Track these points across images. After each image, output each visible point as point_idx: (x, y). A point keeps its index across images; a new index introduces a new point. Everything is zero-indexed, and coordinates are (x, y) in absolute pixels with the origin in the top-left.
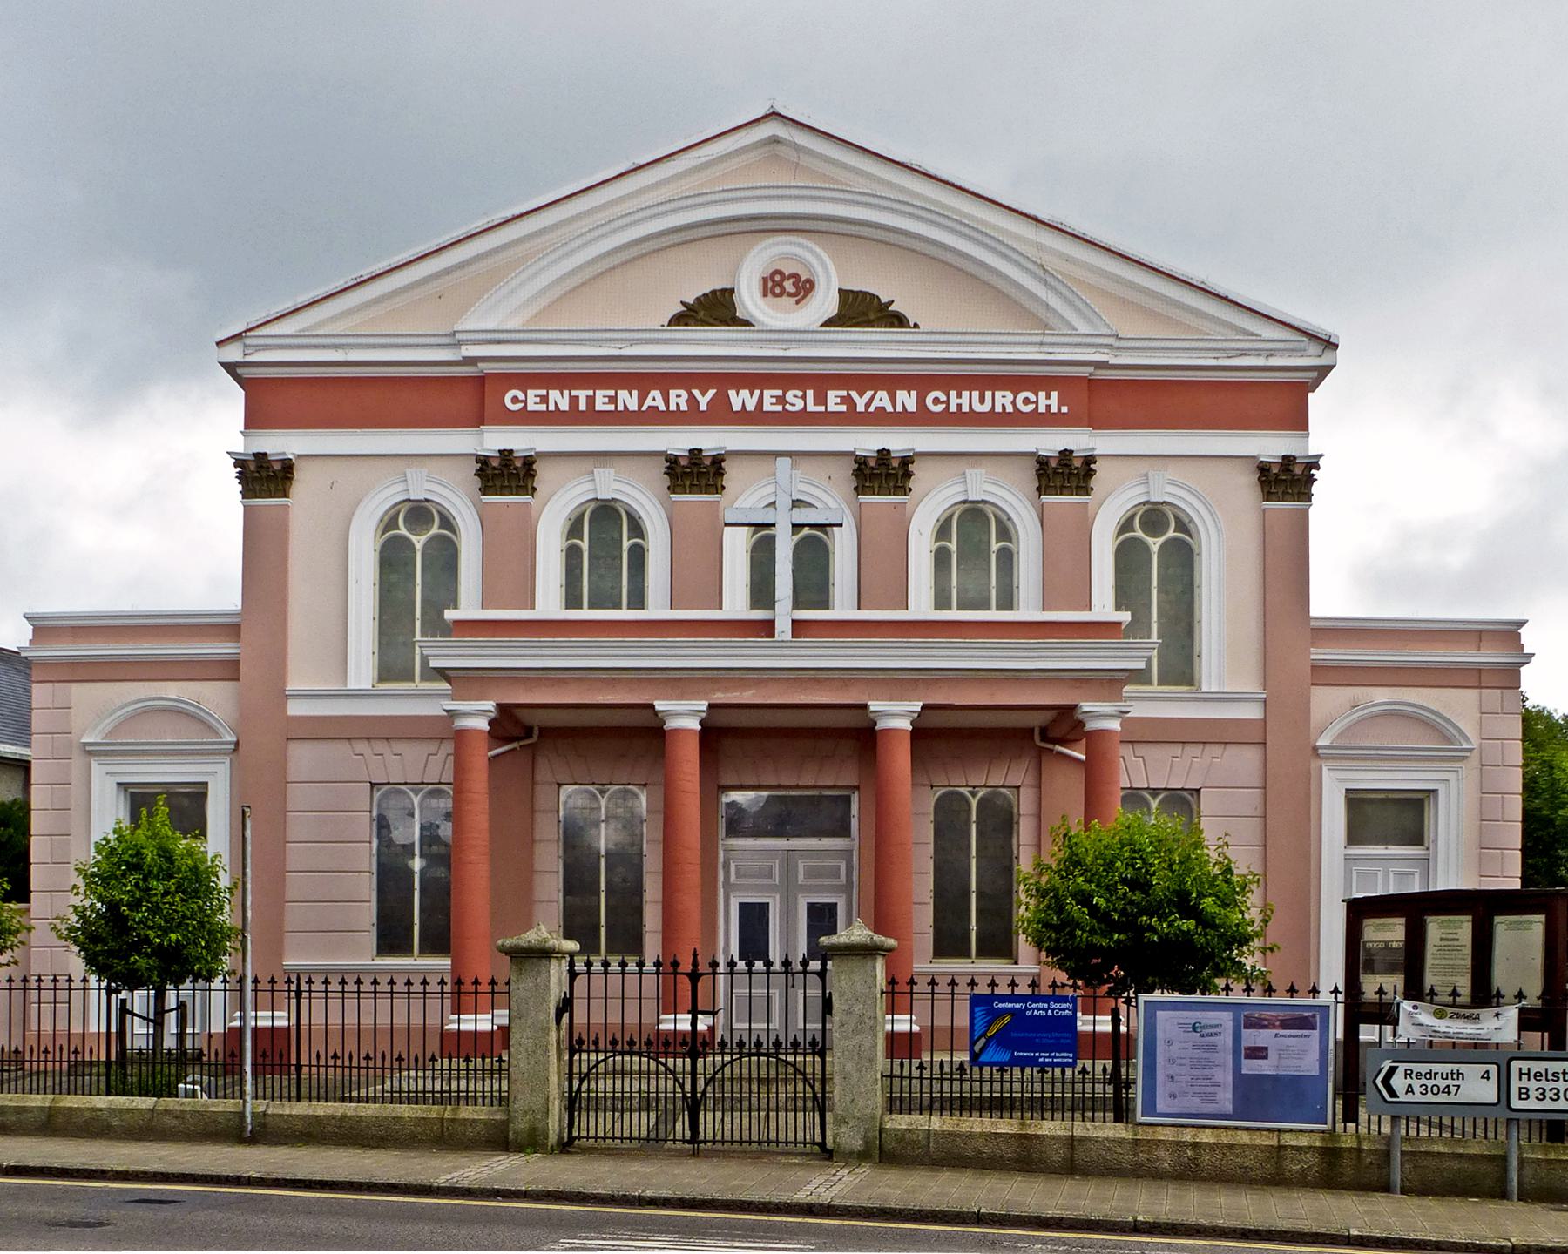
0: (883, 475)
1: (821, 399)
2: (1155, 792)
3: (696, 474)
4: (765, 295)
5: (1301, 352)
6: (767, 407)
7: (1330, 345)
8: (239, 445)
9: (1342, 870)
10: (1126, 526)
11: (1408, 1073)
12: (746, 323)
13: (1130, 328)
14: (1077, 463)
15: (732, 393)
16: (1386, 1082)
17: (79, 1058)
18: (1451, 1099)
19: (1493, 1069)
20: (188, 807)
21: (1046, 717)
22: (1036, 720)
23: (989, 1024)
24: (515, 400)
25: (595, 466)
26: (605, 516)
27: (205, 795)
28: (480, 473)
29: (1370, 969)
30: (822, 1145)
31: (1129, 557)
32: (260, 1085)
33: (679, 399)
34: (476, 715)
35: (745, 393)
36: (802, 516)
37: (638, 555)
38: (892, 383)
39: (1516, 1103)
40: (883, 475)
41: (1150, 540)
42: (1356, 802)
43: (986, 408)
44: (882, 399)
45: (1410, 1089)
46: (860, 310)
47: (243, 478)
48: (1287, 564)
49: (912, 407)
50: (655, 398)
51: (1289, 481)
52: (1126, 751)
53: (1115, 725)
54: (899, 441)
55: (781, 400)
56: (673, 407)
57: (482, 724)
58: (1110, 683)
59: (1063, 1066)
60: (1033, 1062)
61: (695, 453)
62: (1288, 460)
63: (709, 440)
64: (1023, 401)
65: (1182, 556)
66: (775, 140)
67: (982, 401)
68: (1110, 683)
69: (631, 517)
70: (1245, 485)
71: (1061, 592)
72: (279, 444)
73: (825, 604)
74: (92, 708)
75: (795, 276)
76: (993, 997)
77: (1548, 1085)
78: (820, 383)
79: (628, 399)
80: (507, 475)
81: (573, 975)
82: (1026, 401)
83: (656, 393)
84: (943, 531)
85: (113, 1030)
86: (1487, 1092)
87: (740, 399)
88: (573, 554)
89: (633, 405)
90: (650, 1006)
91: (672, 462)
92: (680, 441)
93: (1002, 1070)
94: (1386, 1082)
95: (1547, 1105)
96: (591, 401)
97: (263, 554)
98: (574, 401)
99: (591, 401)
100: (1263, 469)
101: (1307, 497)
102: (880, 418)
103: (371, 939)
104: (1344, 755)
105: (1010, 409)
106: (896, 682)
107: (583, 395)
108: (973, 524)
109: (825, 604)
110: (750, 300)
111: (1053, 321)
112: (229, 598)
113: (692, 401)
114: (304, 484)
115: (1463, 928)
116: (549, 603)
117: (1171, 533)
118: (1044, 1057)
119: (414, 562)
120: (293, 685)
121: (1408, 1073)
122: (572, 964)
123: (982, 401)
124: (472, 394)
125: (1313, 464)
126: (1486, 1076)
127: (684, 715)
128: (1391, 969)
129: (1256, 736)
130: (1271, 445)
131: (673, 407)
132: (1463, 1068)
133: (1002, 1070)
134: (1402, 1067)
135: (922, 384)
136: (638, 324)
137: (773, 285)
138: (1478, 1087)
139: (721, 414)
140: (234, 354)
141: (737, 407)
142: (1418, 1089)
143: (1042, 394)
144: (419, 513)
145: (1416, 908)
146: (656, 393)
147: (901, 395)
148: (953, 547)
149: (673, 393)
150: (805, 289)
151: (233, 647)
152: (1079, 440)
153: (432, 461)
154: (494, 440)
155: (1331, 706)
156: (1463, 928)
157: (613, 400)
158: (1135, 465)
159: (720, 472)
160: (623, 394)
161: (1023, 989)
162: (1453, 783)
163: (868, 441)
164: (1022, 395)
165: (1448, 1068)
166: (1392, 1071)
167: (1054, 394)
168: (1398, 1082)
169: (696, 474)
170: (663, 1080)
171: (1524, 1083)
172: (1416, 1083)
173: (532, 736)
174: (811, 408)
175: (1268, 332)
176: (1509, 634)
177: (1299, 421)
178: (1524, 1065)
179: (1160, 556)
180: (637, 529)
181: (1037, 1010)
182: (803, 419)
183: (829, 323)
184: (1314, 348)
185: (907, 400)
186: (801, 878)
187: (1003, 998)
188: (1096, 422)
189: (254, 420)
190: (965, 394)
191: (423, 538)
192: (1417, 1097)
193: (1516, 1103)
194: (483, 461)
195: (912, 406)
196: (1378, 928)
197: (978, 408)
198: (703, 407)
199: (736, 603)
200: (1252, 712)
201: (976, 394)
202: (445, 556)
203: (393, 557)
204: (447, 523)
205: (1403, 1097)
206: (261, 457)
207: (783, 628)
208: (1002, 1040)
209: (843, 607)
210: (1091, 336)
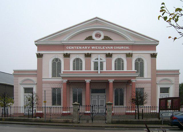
0: (109, 56)
1: (102, 48)
2: (57, 88)
3: (88, 56)
4: (96, 36)
5: (156, 42)
8: (37, 52)
9: (159, 95)
10: (136, 60)
13: (137, 40)
14: (131, 54)
20: (59, 89)
21: (127, 81)
22: (126, 81)
28: (64, 55)
31: (136, 64)
33: (86, 47)
36: (101, 61)
40: (109, 56)
41: (139, 62)
42: (161, 89)
44: (109, 47)
46: (106, 38)
47: (37, 56)
51: (154, 56)
52: (136, 84)
54: (111, 52)
55: (98, 48)
56: (85, 48)
58: (135, 77)
61: (88, 53)
63: (90, 52)
64: (125, 48)
65: (142, 64)
66: (97, 20)
68: (135, 77)
69: (80, 60)
70: (149, 56)
71: (128, 69)
72: (41, 52)
74: (21, 79)
79: (80, 48)
80: (67, 56)
82: (125, 48)
84: (116, 61)
89: (81, 48)
90: (61, 111)
91: (106, 54)
92: (86, 52)
96: (76, 48)
98: (74, 48)
99: (76, 48)
101: (156, 57)
102: (108, 49)
103: (51, 104)
104: (160, 84)
107: (75, 47)
108: (119, 61)
110: (94, 37)
112: (35, 68)
113: (88, 48)
114: (44, 56)
116: (71, 70)
120: (43, 78)
124: (63, 46)
125: (156, 54)
130: (152, 52)
131: (85, 48)
136: (81, 40)
139: (91, 49)
140: (36, 43)
144: (57, 60)
145: (167, 99)
146: (109, 47)
147: (111, 47)
148: (117, 63)
150: (100, 36)
151: (38, 73)
152: (130, 52)
153: (59, 54)
154: (65, 52)
155: (159, 79)
158: (137, 54)
159: (112, 55)
160: (80, 47)
163: (108, 52)
169: (88, 56)
170: (89, 117)
173: (75, 84)
175: (152, 40)
176: (178, 71)
177: (155, 50)
182: (100, 50)
183: (103, 40)
185: (112, 48)
188: (132, 50)
189: (38, 50)
197: (120, 48)
198: (89, 48)
199: (92, 70)
200: (150, 80)
202: (60, 64)
204: (60, 60)
206: (39, 54)
207: (99, 73)
210: (131, 40)
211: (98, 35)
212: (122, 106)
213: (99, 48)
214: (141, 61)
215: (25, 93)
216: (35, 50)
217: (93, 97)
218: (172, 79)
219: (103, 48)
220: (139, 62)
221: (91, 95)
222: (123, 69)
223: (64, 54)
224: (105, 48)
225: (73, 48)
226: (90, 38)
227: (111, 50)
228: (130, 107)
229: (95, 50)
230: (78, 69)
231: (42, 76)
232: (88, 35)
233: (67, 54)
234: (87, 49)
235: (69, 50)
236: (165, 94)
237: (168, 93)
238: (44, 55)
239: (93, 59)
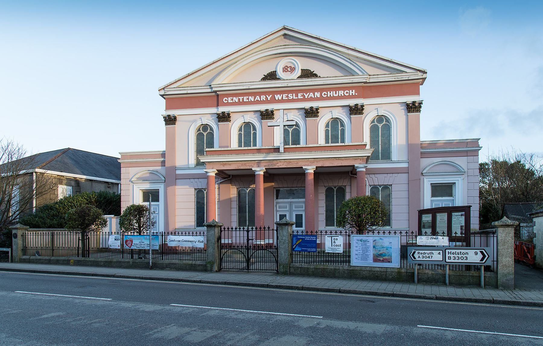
1: (297, 96)
2: (380, 186)
6: (284, 98)
7: (425, 72)
8: (166, 113)
10: (373, 121)
11: (419, 253)
12: (279, 79)
15: (276, 96)
16: (413, 255)
17: (345, 254)
18: (430, 259)
19: (441, 252)
23: (297, 242)
24: (226, 100)
25: (242, 115)
26: (335, 121)
27: (159, 192)
29: (424, 227)
30: (277, 271)
31: (374, 129)
32: (402, 263)
33: (263, 98)
34: (212, 173)
35: (278, 95)
37: (255, 134)
38: (313, 91)
39: (447, 260)
41: (379, 125)
43: (337, 95)
44: (311, 95)
45: (419, 257)
47: (165, 120)
48: (412, 130)
49: (319, 96)
50: (258, 98)
53: (364, 170)
54: (315, 104)
55: (288, 97)
57: (214, 174)
59: (314, 252)
60: (307, 251)
62: (414, 103)
63: (270, 107)
65: (387, 128)
67: (336, 94)
72: (172, 113)
73: (299, 144)
75: (291, 67)
76: (297, 235)
77: (456, 256)
78: (297, 92)
79: (252, 99)
81: (221, 231)
83: (258, 97)
84: (327, 126)
85: (80, 246)
86: (440, 258)
87: (278, 97)
88: (240, 135)
93: (300, 252)
94: (413, 255)
95: (460, 261)
96: (243, 99)
97: (170, 140)
99: (243, 99)
100: (408, 105)
102: (311, 99)
105: (343, 95)
106: (259, 162)
107: (241, 98)
109: (299, 144)
110: (280, 73)
111: (353, 73)
113: (267, 98)
115: (445, 216)
117: (384, 123)
118: (309, 250)
119: (205, 139)
121: (419, 253)
122: (221, 229)
123: (336, 94)
124: (216, 98)
125: (420, 103)
126: (439, 253)
127: (260, 171)
128: (429, 227)
129: (406, 171)
130: (409, 99)
132: (433, 252)
133: (300, 252)
134: (417, 252)
135: (321, 90)
137: (285, 69)
138: (437, 256)
140: (162, 92)
141: (277, 99)
142: (421, 257)
143: (351, 91)
144: (205, 127)
147: (316, 93)
148: (243, 133)
149: (262, 96)
150: (293, 69)
152: (359, 101)
153: (206, 115)
156: (445, 216)
157: (248, 99)
158: (374, 107)
160: (250, 97)
161: (300, 233)
162: (460, 181)
163: (307, 105)
164: (346, 92)
165: (429, 252)
166: (414, 252)
167: (354, 91)
168: (416, 255)
171: (450, 255)
172: (421, 256)
176: (475, 142)
178: (450, 251)
179: (382, 127)
180: (255, 129)
181: (307, 238)
182: (293, 101)
184: (420, 74)
185: (318, 95)
186: (294, 209)
187: (300, 236)
188: (364, 97)
189: (167, 108)
190: (332, 92)
191: (292, 129)
192: (421, 259)
193: (447, 260)
194: (218, 114)
196: (426, 217)
197: (335, 95)
200: (405, 165)
201: (334, 92)
203: (199, 137)
204: (211, 129)
205: (417, 259)
206: (169, 116)
208: (299, 245)
211: (289, 69)
212: (388, 228)
213: (290, 96)
214: (209, 131)
216: (160, 108)
218: (461, 162)
219: (300, 96)
220: (380, 126)
224: (303, 96)
225: (237, 101)
227: (317, 99)
228: (107, 232)
229: (282, 101)
230: (247, 144)
233: (223, 113)
234: (267, 102)
235: (228, 104)
236: (444, 198)
237: (451, 195)
238: (178, 118)
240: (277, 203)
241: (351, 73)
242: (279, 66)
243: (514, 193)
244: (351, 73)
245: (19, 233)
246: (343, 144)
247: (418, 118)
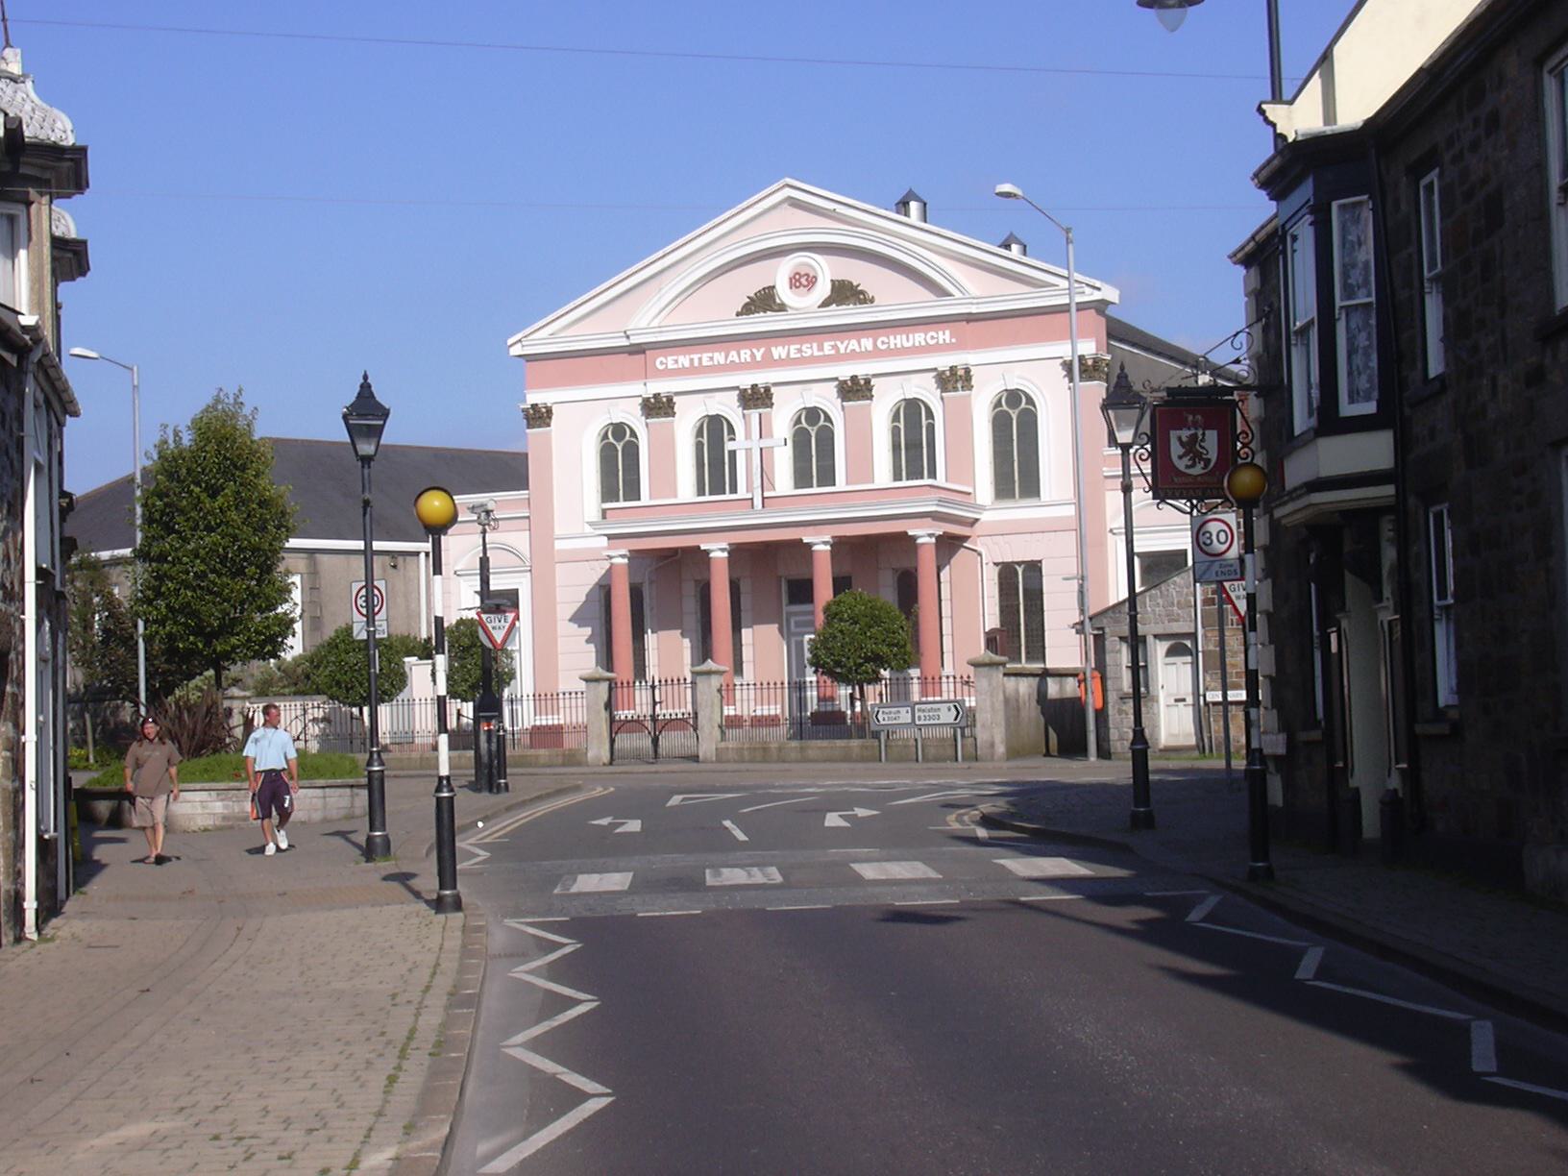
2: (1019, 563)
37: (931, 428)
46: (844, 293)
54: (861, 369)
55: (800, 351)
87: (778, 352)
88: (895, 432)
102: (853, 356)
107: (696, 357)
110: (784, 293)
113: (753, 355)
120: (558, 532)
139: (769, 362)
144: (619, 430)
146: (734, 353)
153: (621, 400)
155: (1347, 409)
174: (816, 353)
182: (813, 360)
183: (825, 304)
195: (870, 348)
202: (632, 451)
203: (607, 455)
209: (841, 483)
215: (1013, 496)
217: (797, 624)
221: (789, 614)
222: (734, 490)
223: (646, 401)
226: (764, 301)
229: (787, 362)
231: (552, 529)
232: (749, 282)
234: (753, 365)
239: (687, 419)
240: (789, 614)
241: (941, 292)
242: (779, 274)
243: (1431, 381)
244: (941, 292)
245: (236, 705)
246: (733, 496)
247: (549, 433)
